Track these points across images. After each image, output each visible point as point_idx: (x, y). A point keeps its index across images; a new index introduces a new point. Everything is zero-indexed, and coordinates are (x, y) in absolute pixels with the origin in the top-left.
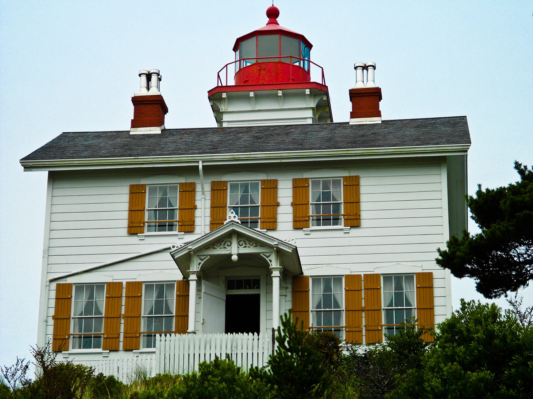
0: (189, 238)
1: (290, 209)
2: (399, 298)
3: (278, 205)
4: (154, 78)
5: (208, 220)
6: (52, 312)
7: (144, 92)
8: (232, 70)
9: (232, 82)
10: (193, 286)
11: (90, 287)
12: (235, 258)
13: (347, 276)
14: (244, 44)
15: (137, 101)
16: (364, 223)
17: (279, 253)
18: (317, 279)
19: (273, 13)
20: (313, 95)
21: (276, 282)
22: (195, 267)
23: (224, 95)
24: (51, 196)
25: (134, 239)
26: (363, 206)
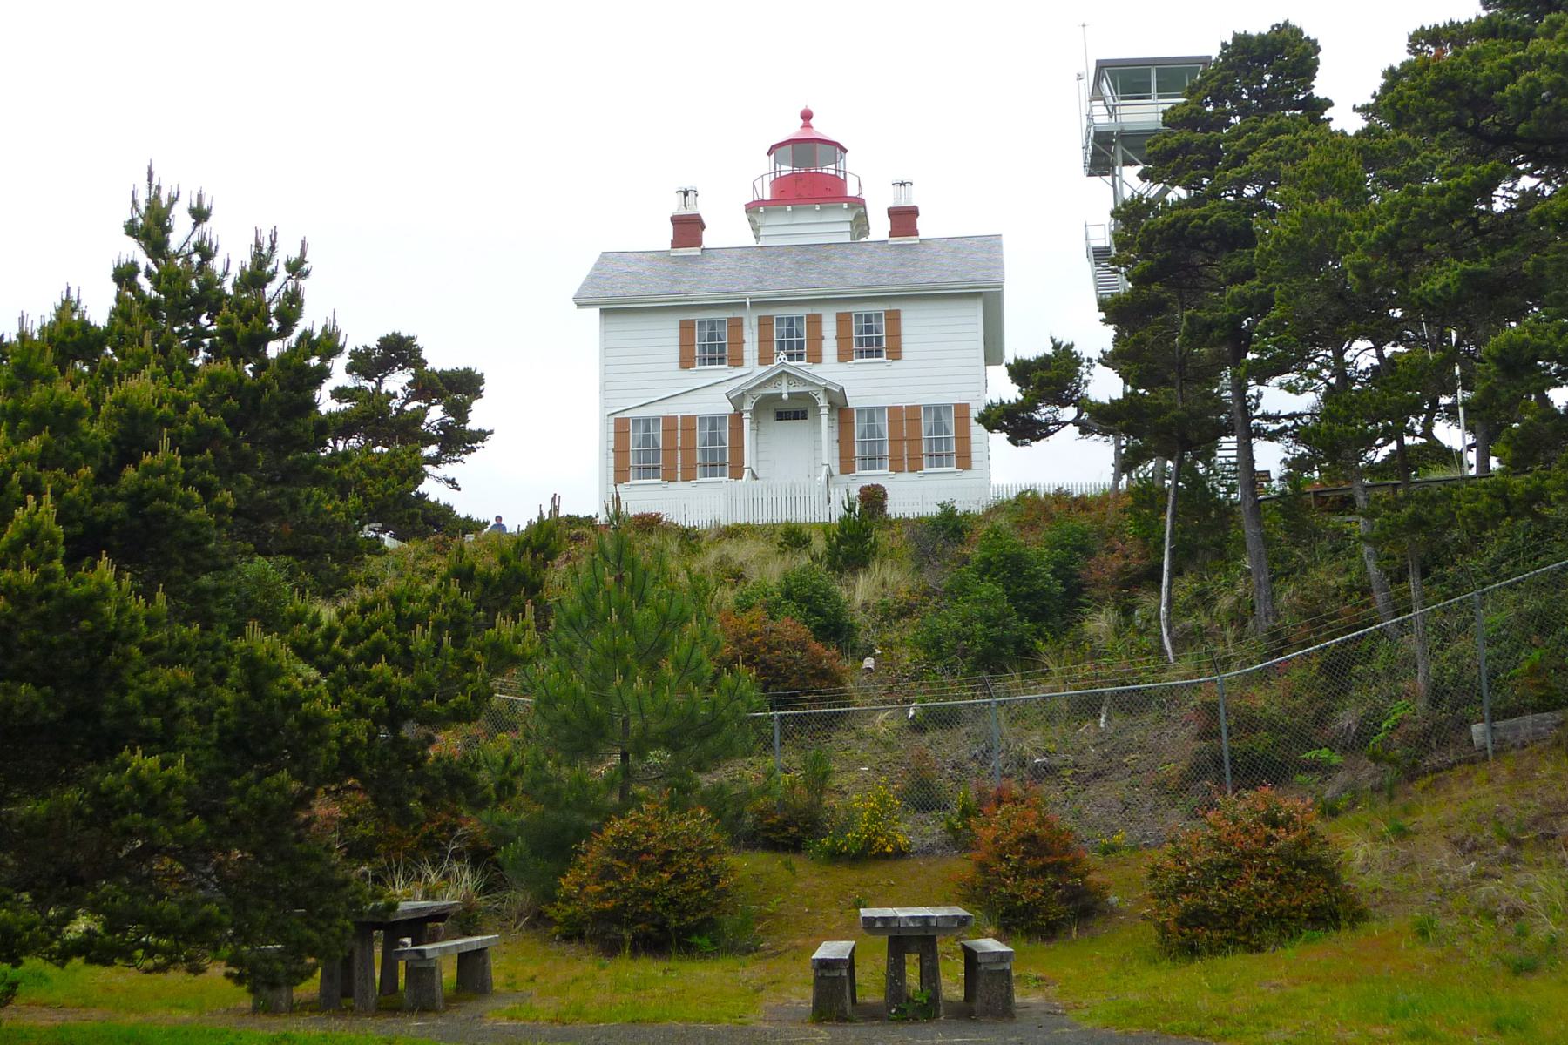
0: (739, 371)
1: (835, 343)
2: (938, 428)
3: (823, 338)
4: (691, 195)
5: (756, 354)
6: (612, 445)
7: (683, 212)
8: (768, 180)
9: (767, 197)
10: (747, 423)
11: (647, 421)
12: (785, 396)
13: (889, 408)
14: (779, 150)
15: (677, 221)
16: (905, 355)
17: (826, 390)
18: (860, 411)
19: (807, 116)
20: (851, 208)
21: (824, 411)
22: (748, 406)
23: (761, 209)
24: (604, 332)
25: (686, 373)
26: (904, 339)
